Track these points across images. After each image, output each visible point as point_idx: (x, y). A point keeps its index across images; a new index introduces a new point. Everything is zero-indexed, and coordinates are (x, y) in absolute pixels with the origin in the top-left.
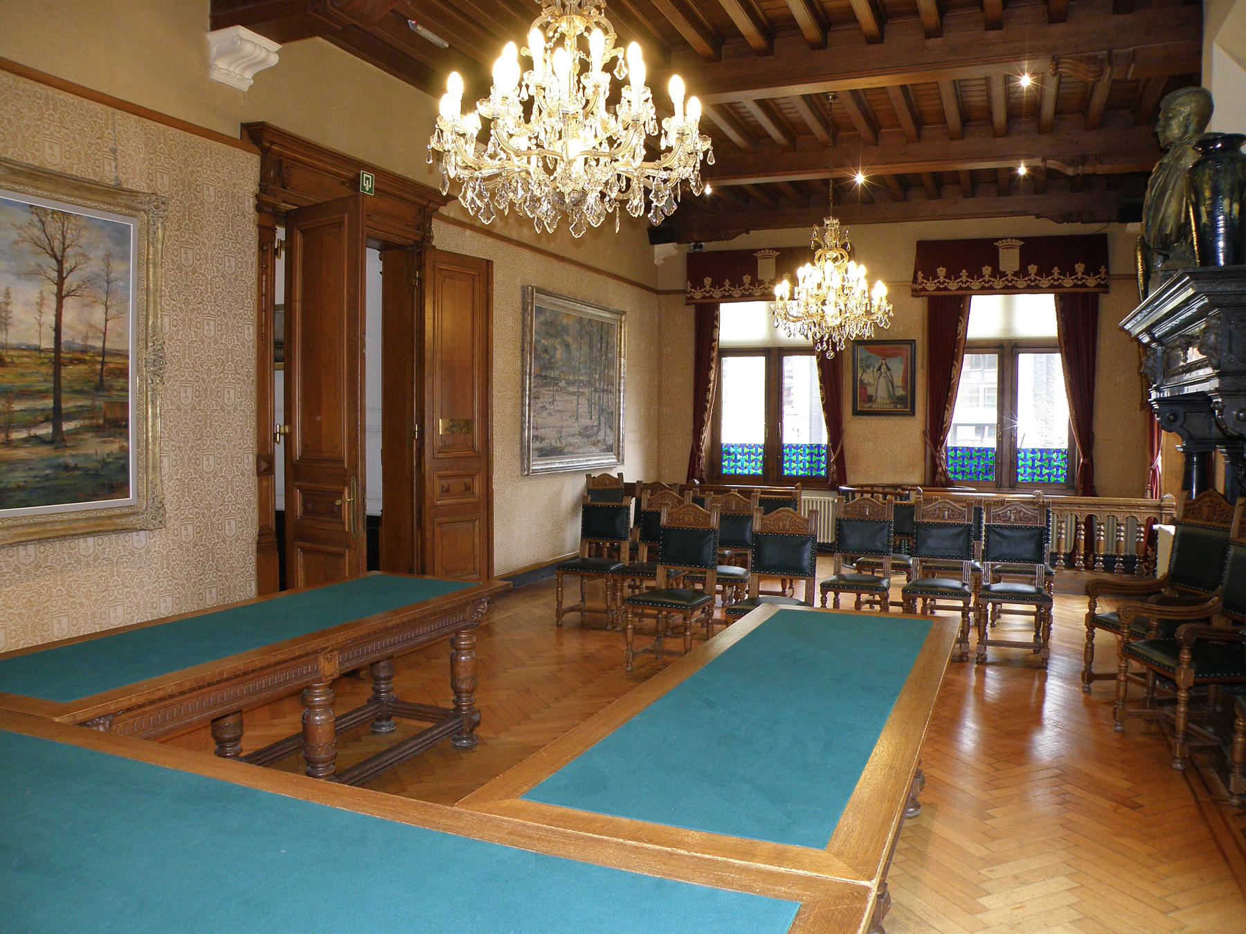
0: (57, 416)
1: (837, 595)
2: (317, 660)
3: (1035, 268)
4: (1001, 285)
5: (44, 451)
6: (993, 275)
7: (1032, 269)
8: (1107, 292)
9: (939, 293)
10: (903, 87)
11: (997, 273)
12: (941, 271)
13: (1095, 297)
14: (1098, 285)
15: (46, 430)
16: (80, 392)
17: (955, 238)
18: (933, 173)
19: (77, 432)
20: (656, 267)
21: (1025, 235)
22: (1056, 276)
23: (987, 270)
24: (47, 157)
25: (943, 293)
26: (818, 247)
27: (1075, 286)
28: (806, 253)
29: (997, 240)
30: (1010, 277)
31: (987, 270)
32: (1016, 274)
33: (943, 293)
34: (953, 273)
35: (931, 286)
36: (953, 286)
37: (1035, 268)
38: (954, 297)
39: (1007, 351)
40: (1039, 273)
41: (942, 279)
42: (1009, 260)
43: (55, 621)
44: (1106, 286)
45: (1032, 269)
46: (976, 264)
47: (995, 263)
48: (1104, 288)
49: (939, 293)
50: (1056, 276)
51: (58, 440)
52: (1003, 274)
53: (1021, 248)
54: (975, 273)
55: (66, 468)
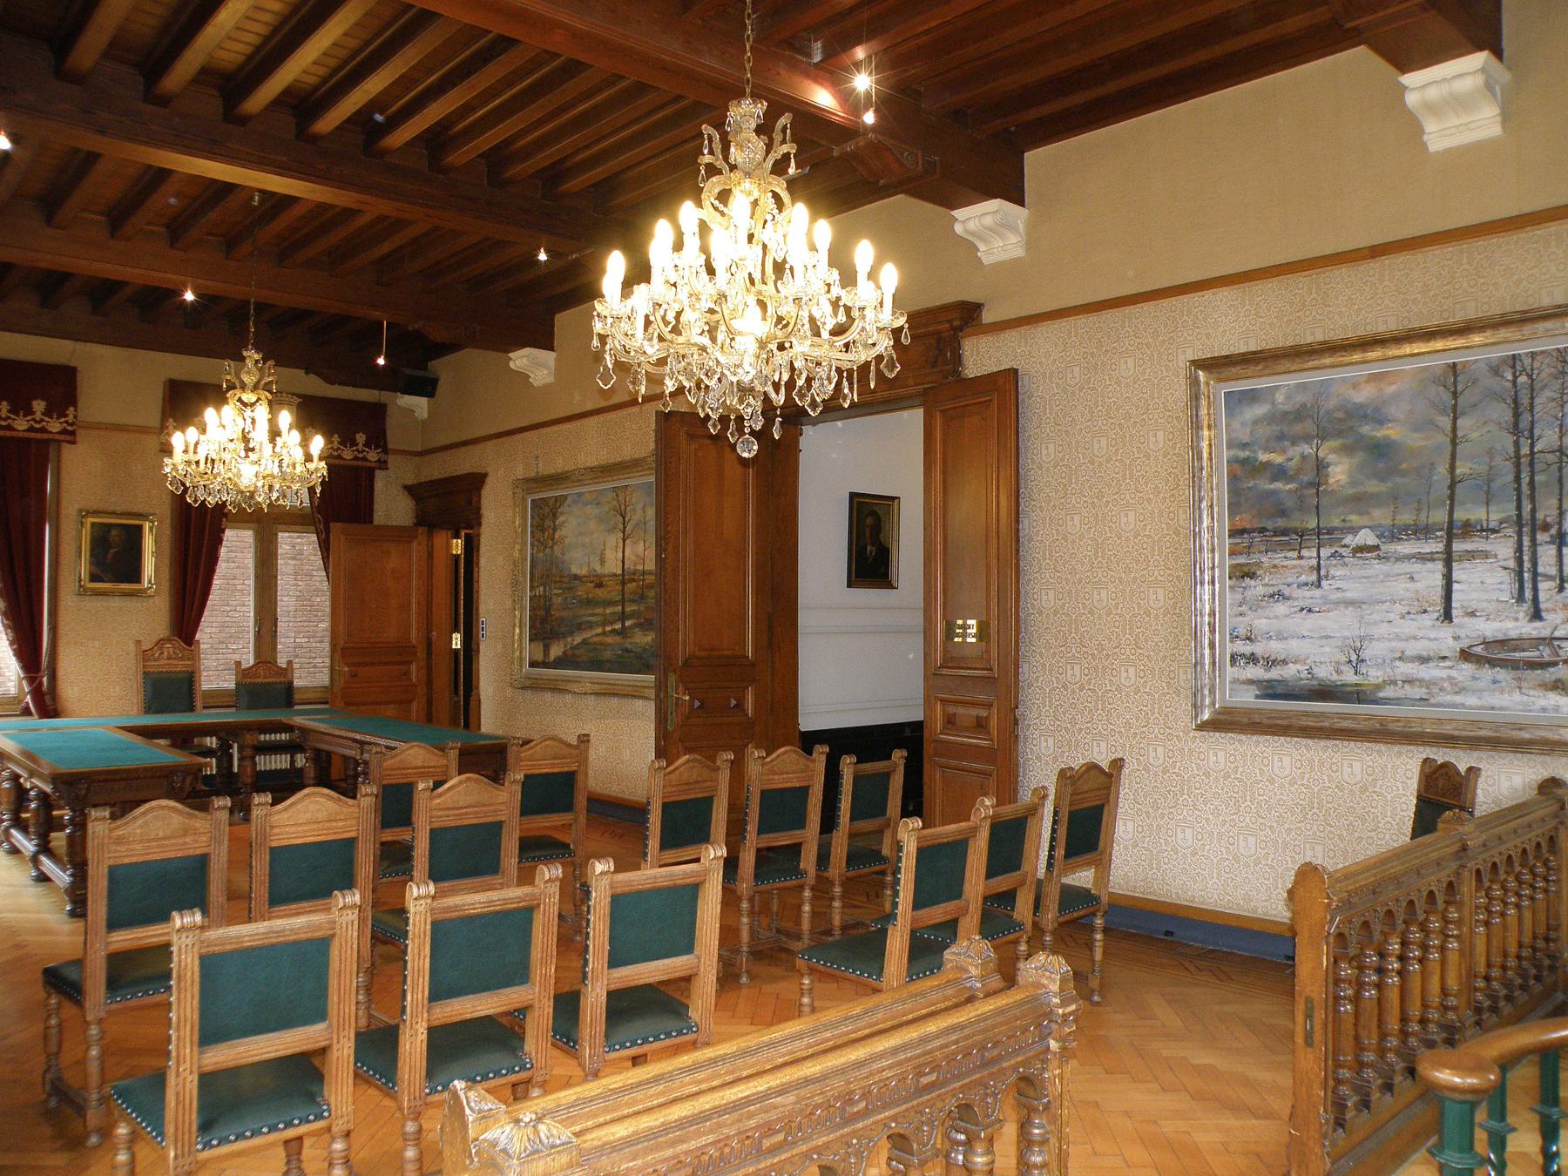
0: (623, 617)
5: (618, 639)
8: (74, 443)
9: (33, 435)
13: (370, 474)
14: (64, 432)
15: (618, 626)
16: (634, 601)
17: (21, 357)
19: (631, 627)
25: (39, 436)
26: (232, 387)
27: (356, 458)
28: (216, 394)
33: (39, 436)
38: (19, 440)
43: (1503, 777)
44: (73, 433)
48: (70, 435)
49: (33, 435)
51: (623, 633)
55: (627, 650)
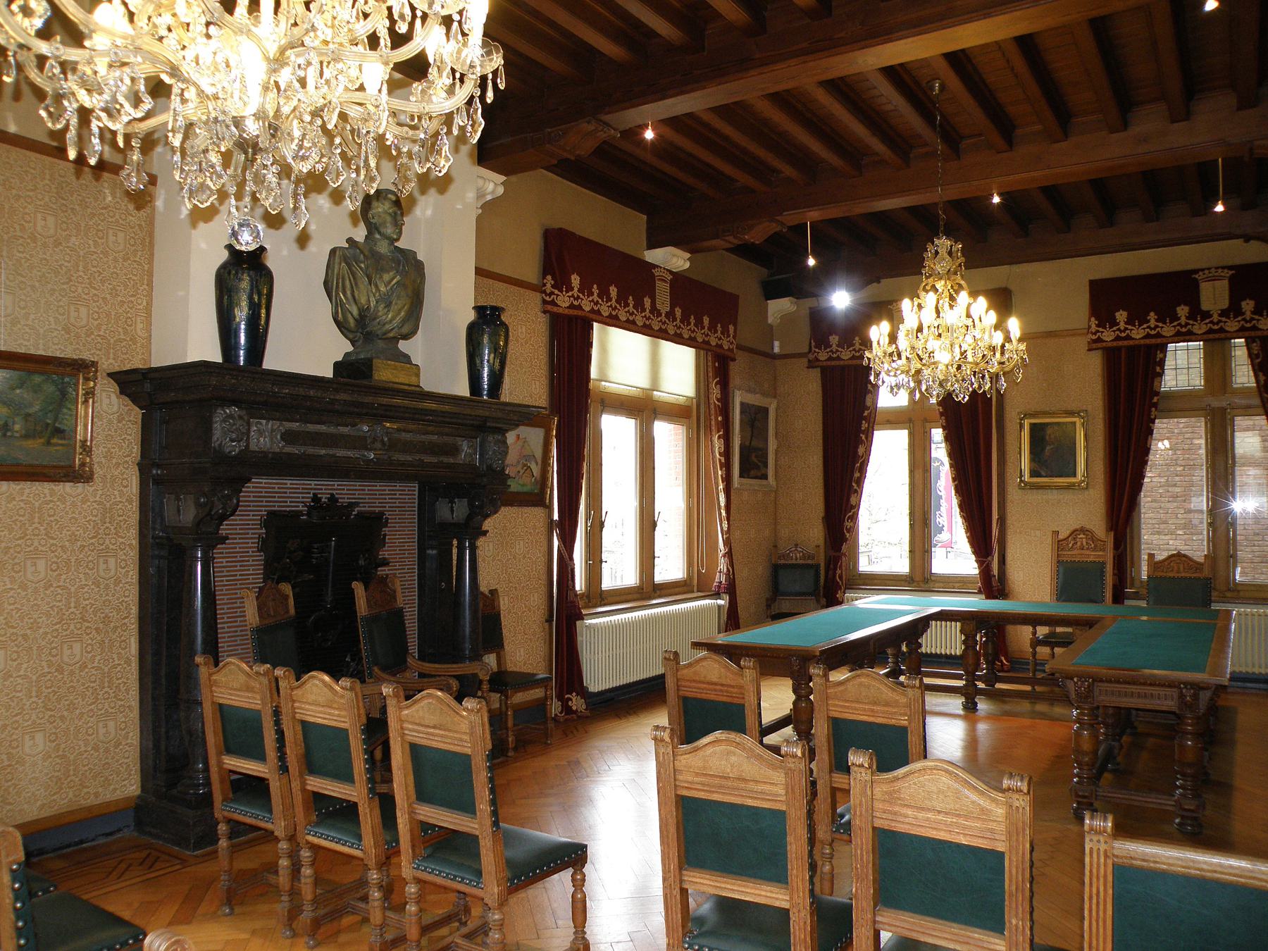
1: (1034, 628)
2: (76, 376)
3: (1125, 314)
4: (1204, 328)
6: (1191, 316)
7: (1248, 306)
10: (1026, 43)
11: (1197, 313)
12: (1121, 316)
18: (1090, 181)
20: (771, 327)
21: (1237, 262)
22: (1152, 323)
23: (1183, 311)
24: (111, 245)
25: (1125, 343)
29: (1196, 271)
30: (1215, 318)
31: (1183, 311)
32: (1224, 313)
34: (1137, 318)
35: (1108, 335)
36: (1138, 333)
37: (1125, 314)
39: (643, 408)
40: (1129, 321)
41: (1122, 326)
42: (1214, 296)
45: (1248, 306)
46: (1169, 299)
47: (1192, 298)
50: (1152, 323)
52: (1207, 315)
53: (1231, 279)
54: (1167, 315)
